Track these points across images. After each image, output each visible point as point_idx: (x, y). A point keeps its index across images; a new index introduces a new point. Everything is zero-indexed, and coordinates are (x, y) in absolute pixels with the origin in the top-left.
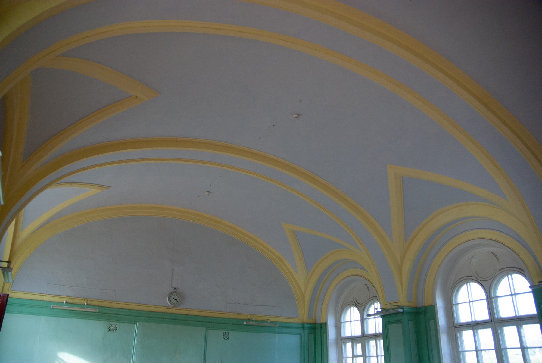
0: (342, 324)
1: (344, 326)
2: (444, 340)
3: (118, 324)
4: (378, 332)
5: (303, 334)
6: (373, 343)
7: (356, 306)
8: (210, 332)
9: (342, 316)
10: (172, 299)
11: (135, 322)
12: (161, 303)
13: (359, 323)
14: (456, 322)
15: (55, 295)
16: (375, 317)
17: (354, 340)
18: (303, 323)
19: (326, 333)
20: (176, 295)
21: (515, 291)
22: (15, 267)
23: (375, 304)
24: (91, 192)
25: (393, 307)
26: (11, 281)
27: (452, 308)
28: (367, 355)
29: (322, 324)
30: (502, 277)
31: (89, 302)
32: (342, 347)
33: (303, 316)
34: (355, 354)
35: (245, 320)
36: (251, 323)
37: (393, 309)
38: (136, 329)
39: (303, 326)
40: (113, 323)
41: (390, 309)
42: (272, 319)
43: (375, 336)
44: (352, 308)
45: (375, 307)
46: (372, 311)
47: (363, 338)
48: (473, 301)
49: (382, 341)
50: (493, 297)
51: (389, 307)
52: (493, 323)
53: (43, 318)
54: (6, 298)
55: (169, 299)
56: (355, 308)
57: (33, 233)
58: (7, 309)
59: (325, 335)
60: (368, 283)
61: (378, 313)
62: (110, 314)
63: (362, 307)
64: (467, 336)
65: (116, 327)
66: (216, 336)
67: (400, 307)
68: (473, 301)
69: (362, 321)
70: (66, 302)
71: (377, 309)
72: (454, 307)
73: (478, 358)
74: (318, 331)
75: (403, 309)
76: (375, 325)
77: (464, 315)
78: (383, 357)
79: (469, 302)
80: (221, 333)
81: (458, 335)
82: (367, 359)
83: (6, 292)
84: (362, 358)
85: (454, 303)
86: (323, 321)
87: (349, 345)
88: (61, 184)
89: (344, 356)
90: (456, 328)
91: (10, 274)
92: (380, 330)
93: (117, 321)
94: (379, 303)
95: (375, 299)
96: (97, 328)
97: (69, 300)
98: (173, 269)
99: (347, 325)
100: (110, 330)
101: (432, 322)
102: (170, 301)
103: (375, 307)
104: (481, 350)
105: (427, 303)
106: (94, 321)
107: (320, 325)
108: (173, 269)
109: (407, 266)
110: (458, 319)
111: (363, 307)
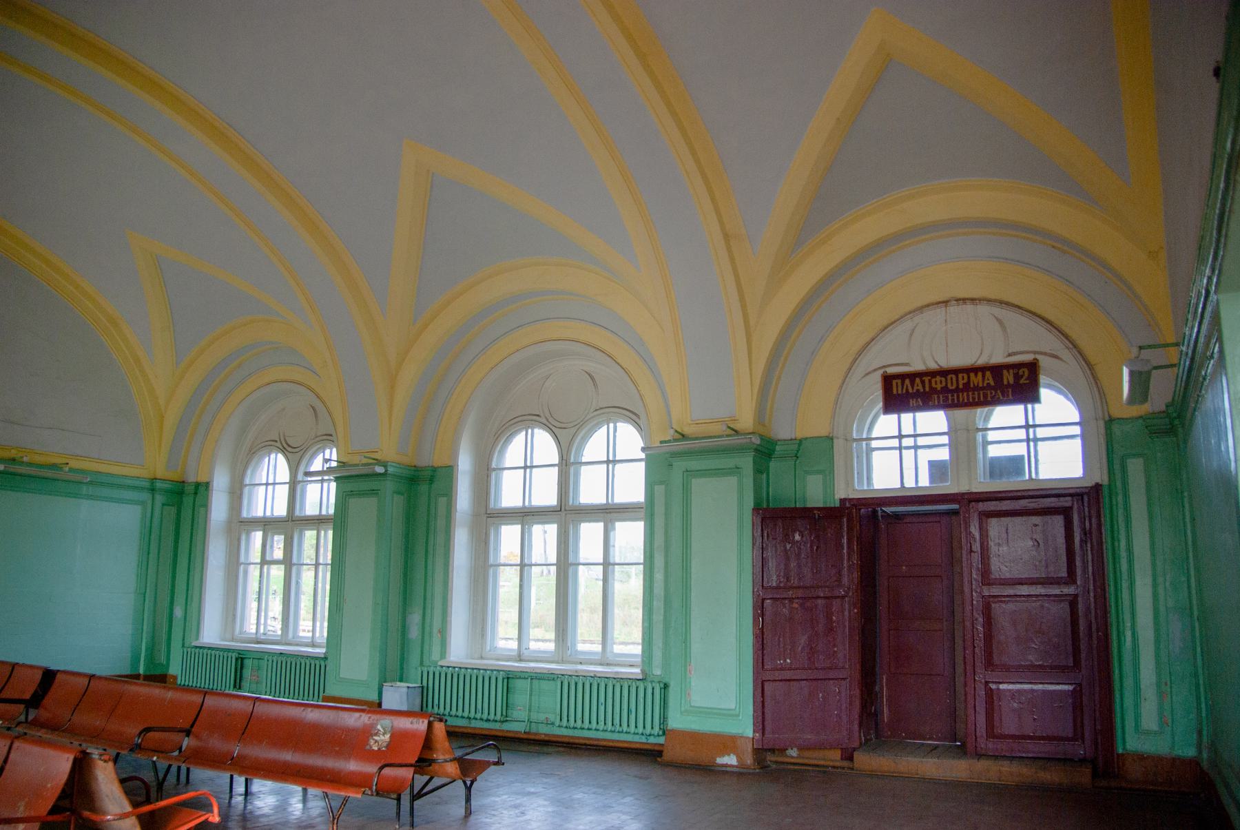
17: (527, 516)
18: (153, 480)
21: (614, 455)
27: (488, 476)
29: (198, 485)
48: (1035, 426)
68: (532, 467)
86: (202, 478)
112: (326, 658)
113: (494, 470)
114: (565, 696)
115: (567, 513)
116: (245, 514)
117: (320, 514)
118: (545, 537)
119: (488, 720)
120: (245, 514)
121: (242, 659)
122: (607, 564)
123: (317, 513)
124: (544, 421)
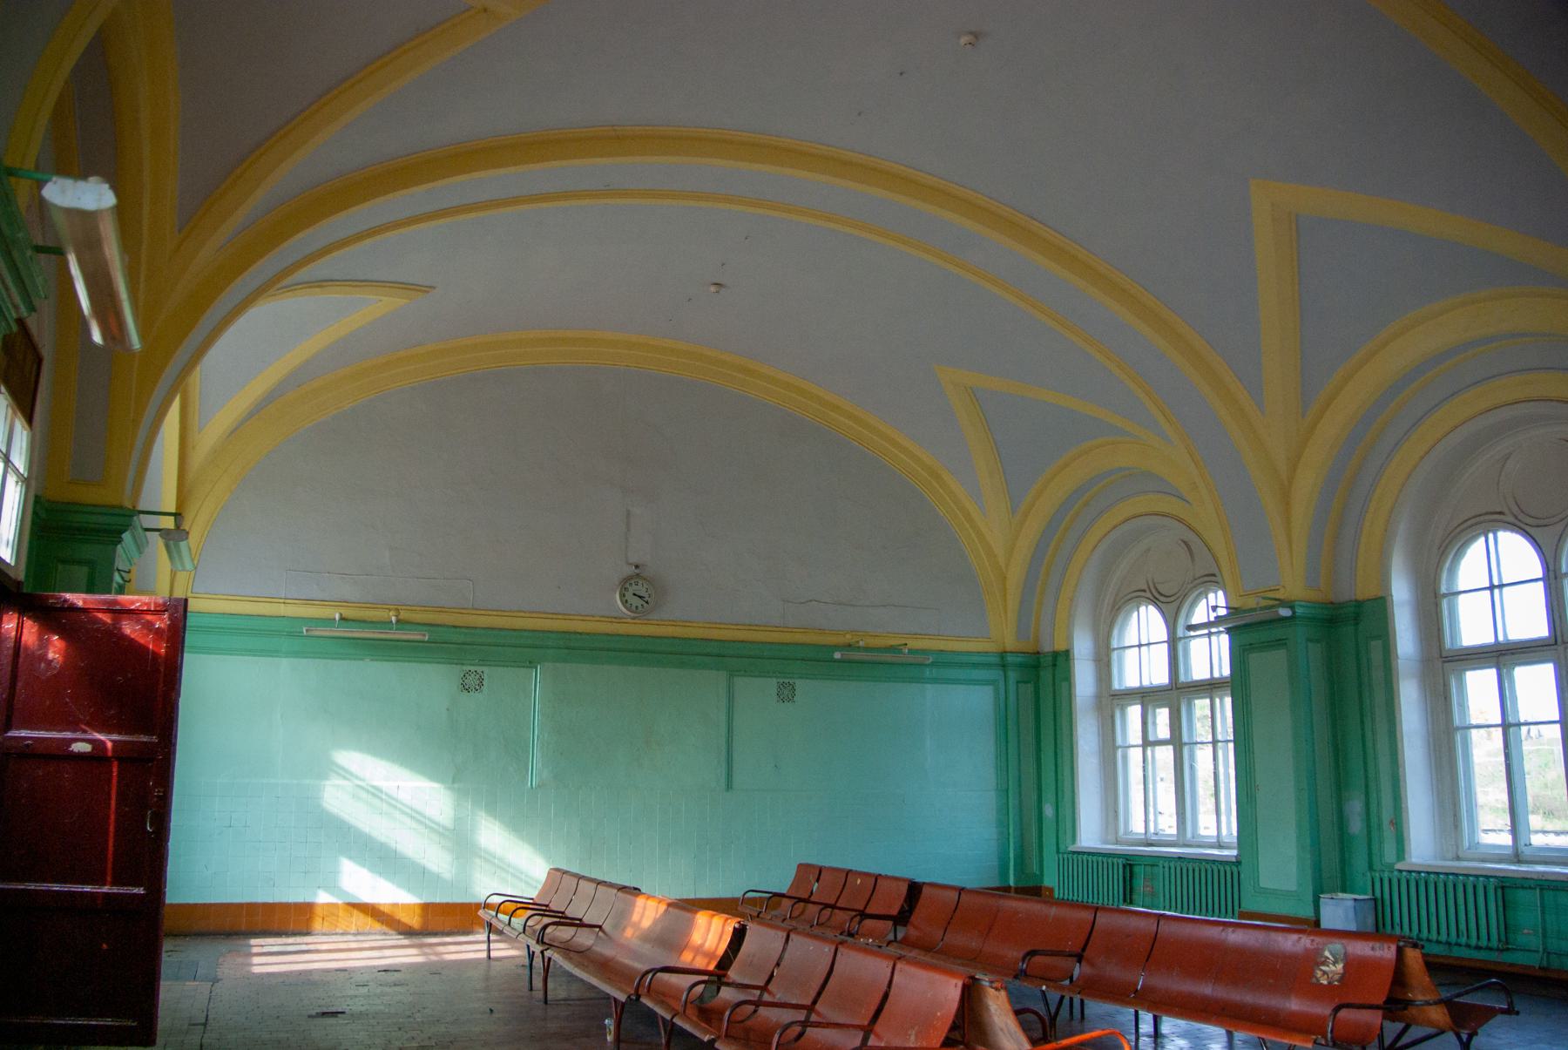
0: (1115, 655)
1: (1120, 660)
2: (1409, 696)
3: (485, 669)
4: (1216, 675)
5: (1002, 684)
6: (1201, 706)
7: (1155, 601)
8: (740, 682)
9: (1115, 632)
10: (629, 596)
11: (531, 664)
12: (604, 611)
13: (1162, 651)
14: (1448, 644)
15: (308, 601)
16: (1210, 635)
17: (1147, 696)
18: (1003, 654)
19: (1068, 678)
20: (640, 587)
22: (197, 526)
23: (1211, 596)
24: (375, 307)
25: (1264, 603)
26: (189, 566)
27: (1437, 605)
28: (1185, 739)
29: (1056, 655)
31: (404, 615)
32: (1113, 717)
33: (1004, 633)
34: (1151, 738)
35: (836, 647)
36: (856, 656)
37: (1267, 608)
38: (536, 684)
39: (1002, 661)
40: (473, 668)
41: (1254, 610)
42: (914, 644)
43: (1210, 687)
44: (1142, 609)
45: (1210, 605)
46: (1200, 614)
47: (1175, 693)
49: (1228, 701)
50: (1445, 595)
51: (1251, 602)
52: (1561, 648)
53: (285, 663)
54: (181, 609)
55: (622, 596)
56: (1151, 608)
57: (234, 431)
58: (187, 644)
59: (1064, 684)
60: (1190, 536)
61: (1219, 620)
62: (460, 644)
63: (1172, 604)
64: (1480, 686)
65: (481, 680)
66: (757, 692)
67: (1283, 603)
69: (1173, 643)
70: (342, 619)
71: (1215, 608)
72: (1445, 603)
73: (1507, 756)
74: (1046, 675)
75: (1292, 608)
76: (1210, 656)
77: (1473, 625)
78: (1231, 745)
79: (1491, 588)
80: (772, 684)
82: (1186, 750)
83: (179, 594)
84: (1170, 747)
85: (1443, 590)
86: (1060, 646)
87: (1134, 712)
88: (289, 288)
89: (1119, 741)
90: (1446, 662)
91: (183, 544)
93: (484, 661)
94: (1220, 593)
95: (1210, 580)
96: (431, 683)
97: (350, 613)
98: (628, 514)
99: (1131, 656)
100: (466, 688)
101: (1376, 645)
102: (625, 603)
103: (1210, 605)
104: (1519, 725)
105: (1363, 590)
106: (428, 666)
108: (628, 514)
109: (1307, 482)
111: (1175, 605)
116: (1116, 686)
119: (1478, 948)
123: (1491, 640)
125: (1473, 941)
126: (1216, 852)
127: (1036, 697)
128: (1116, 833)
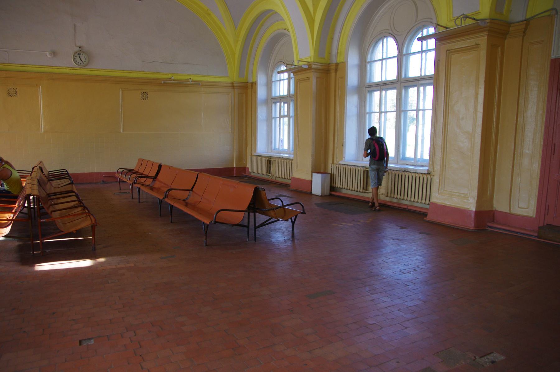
17: (384, 85)
18: (232, 83)
19: (344, 78)
21: (387, 55)
27: (365, 66)
29: (252, 83)
30: (377, 42)
32: (272, 107)
33: (233, 76)
43: (281, 99)
48: (387, 59)
68: (387, 59)
74: (249, 91)
81: (368, 95)
86: (254, 80)
89: (368, 110)
92: (430, 70)
98: (75, 25)
99: (377, 66)
102: (75, 62)
107: (334, 67)
108: (75, 25)
110: (406, 74)
112: (429, 174)
113: (368, 62)
114: (393, 179)
115: (402, 83)
116: (273, 95)
117: (382, 81)
118: (392, 94)
119: (357, 191)
120: (273, 95)
121: (367, 171)
122: (380, 112)
123: (380, 80)
124: (390, 32)
125: (359, 190)
126: (413, 167)
127: (244, 98)
128: (271, 148)
